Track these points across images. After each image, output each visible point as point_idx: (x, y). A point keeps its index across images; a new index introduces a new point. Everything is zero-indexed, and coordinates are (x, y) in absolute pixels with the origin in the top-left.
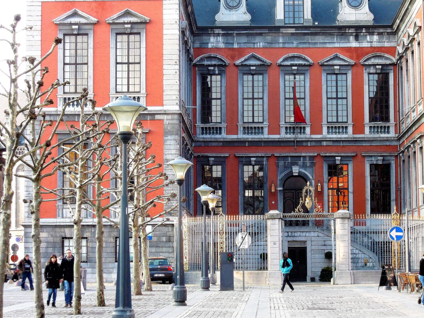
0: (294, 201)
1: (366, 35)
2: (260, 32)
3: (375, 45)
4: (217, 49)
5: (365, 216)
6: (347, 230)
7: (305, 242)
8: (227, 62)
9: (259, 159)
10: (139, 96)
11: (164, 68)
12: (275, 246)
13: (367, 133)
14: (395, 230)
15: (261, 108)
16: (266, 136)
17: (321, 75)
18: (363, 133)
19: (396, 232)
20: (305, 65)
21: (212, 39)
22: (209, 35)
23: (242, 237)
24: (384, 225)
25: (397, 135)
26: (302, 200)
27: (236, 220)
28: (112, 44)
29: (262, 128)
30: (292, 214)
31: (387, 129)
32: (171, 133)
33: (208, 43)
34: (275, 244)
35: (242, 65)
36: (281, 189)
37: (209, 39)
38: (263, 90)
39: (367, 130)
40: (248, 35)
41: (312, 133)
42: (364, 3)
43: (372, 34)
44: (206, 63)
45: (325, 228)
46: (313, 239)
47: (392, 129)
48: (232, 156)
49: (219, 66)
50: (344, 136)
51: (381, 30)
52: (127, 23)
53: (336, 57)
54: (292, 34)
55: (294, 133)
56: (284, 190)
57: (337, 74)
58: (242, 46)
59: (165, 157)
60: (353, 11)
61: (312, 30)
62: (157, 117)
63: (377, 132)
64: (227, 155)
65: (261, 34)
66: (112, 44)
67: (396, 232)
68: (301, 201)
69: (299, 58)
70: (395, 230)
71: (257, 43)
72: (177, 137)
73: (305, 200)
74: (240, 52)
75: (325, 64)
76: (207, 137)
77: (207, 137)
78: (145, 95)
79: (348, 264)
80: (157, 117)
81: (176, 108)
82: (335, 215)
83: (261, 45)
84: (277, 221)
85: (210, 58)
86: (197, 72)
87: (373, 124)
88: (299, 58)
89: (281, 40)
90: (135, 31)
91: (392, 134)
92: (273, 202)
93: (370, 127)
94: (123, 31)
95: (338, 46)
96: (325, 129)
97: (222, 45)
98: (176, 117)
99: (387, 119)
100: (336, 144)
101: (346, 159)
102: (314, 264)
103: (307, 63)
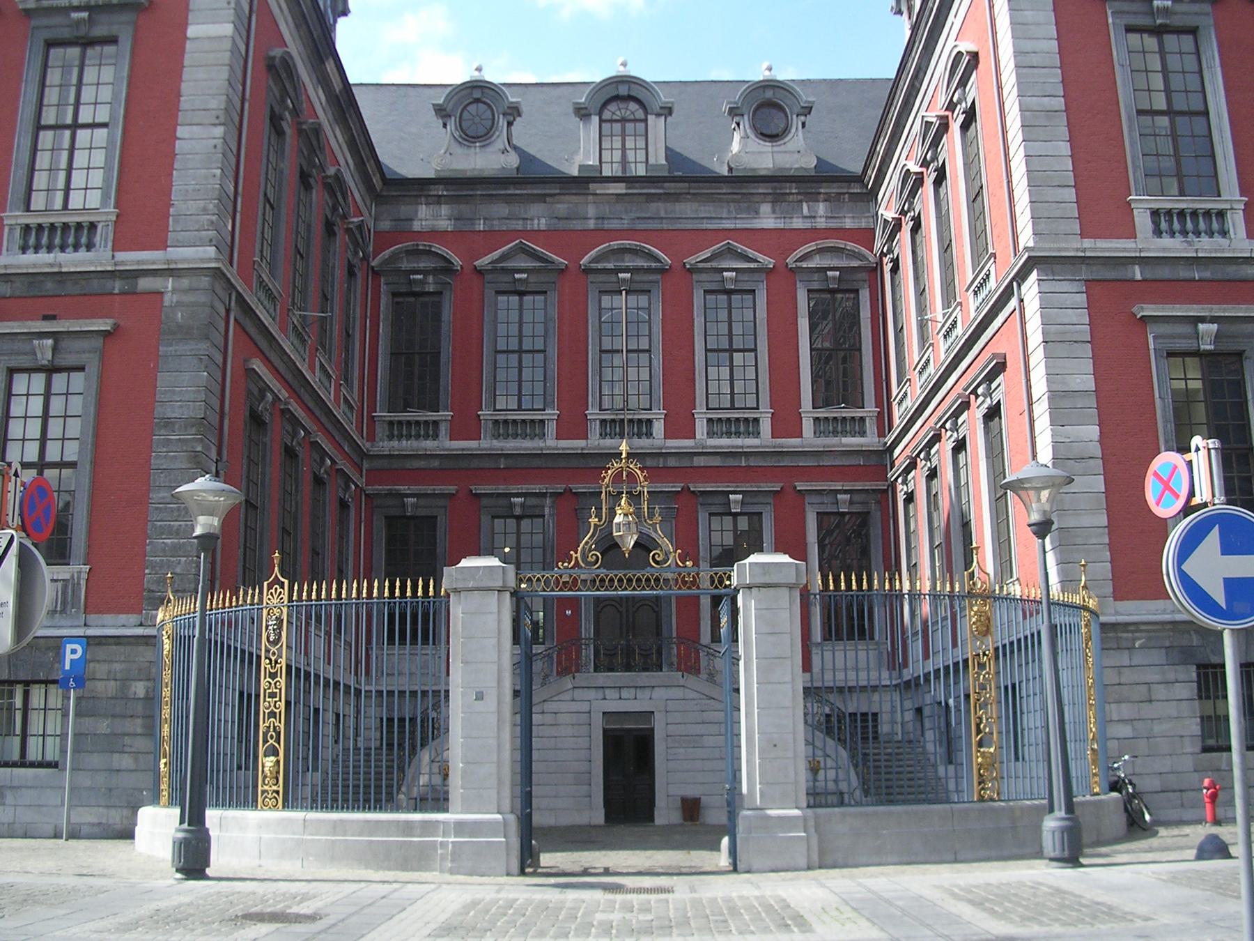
0: (623, 610)
1: (801, 201)
2: (539, 192)
3: (821, 223)
4: (435, 234)
6: (786, 639)
8: (457, 262)
9: (532, 501)
10: (92, 219)
11: (179, 134)
13: (809, 438)
14: (1214, 536)
15: (539, 375)
16: (551, 443)
17: (697, 512)
21: (423, 210)
22: (416, 200)
24: (857, 669)
26: (599, 516)
28: (31, 73)
31: (857, 425)
32: (184, 333)
33: (411, 220)
37: (416, 212)
38: (546, 331)
39: (808, 427)
40: (508, 199)
42: (793, 130)
43: (813, 197)
44: (405, 265)
45: (704, 676)
47: (871, 426)
49: (435, 271)
51: (834, 189)
57: (729, 292)
58: (497, 225)
59: (159, 411)
60: (767, 146)
61: (671, 187)
62: (144, 284)
64: (452, 489)
65: (542, 198)
66: (31, 73)
68: (593, 520)
70: (1214, 536)
71: (532, 219)
72: (203, 347)
73: (612, 514)
74: (493, 238)
75: (701, 265)
76: (408, 446)
77: (408, 446)
78: (114, 218)
80: (144, 284)
81: (206, 255)
82: (735, 575)
83: (543, 224)
85: (415, 253)
86: (383, 287)
87: (822, 413)
89: (591, 211)
90: (99, 31)
92: (569, 612)
94: (65, 33)
95: (732, 226)
96: (701, 428)
97: (445, 224)
98: (205, 281)
100: (730, 462)
101: (755, 500)
102: (671, 779)
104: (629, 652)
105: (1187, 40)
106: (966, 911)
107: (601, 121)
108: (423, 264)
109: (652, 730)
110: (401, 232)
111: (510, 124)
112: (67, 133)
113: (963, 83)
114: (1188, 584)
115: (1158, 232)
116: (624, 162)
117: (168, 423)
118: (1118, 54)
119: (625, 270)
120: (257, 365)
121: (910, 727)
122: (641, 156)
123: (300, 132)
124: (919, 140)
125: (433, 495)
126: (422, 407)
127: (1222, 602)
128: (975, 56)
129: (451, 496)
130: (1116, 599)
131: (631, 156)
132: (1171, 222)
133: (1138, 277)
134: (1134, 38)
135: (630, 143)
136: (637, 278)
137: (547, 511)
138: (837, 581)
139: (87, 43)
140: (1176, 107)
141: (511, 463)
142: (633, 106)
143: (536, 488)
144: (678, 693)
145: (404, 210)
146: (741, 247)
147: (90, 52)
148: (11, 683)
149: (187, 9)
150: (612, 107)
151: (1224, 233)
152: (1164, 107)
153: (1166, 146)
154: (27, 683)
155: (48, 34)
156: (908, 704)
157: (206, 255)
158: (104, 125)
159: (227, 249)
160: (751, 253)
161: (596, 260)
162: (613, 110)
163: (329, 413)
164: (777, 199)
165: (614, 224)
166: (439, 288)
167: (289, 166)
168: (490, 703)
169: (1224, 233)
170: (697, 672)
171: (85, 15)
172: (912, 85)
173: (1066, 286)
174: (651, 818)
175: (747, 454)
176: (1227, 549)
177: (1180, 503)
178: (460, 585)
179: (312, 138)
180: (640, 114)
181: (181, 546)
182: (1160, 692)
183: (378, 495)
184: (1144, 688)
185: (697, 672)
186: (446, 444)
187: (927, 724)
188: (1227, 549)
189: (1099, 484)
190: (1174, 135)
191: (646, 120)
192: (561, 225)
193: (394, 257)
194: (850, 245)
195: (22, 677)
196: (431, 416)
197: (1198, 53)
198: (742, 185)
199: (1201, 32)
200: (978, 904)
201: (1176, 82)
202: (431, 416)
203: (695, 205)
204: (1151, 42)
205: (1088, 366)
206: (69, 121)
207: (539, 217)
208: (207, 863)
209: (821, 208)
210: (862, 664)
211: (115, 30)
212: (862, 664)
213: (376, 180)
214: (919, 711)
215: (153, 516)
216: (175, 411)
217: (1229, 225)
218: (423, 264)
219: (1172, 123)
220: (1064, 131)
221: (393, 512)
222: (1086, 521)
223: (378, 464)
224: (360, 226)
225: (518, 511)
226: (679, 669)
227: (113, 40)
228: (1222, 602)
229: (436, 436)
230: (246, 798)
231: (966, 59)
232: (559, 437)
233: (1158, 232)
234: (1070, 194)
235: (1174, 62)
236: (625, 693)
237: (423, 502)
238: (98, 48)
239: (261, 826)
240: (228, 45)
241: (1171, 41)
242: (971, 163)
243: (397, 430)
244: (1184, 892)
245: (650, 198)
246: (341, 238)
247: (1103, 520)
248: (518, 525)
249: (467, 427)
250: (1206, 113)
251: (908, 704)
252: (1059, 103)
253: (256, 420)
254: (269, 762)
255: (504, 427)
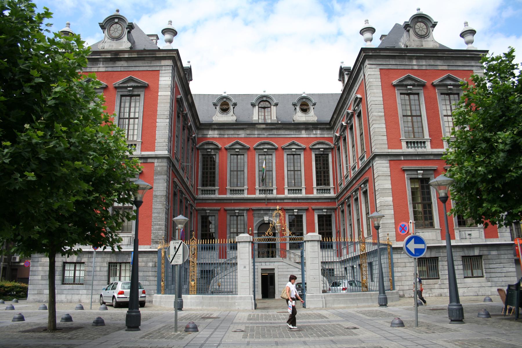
3: (319, 136)
4: (213, 138)
5: (331, 239)
7: (274, 269)
8: (220, 146)
9: (241, 212)
12: (245, 269)
14: (413, 240)
16: (246, 195)
18: (313, 193)
19: (415, 243)
20: (272, 149)
22: (208, 129)
23: (175, 248)
25: (335, 195)
27: (207, 243)
29: (243, 190)
30: (262, 237)
32: (160, 173)
34: (245, 267)
35: (230, 149)
36: (257, 232)
39: (315, 191)
41: (277, 194)
43: (316, 129)
44: (206, 147)
45: (288, 259)
46: (279, 267)
47: (332, 191)
48: (222, 210)
49: (214, 149)
50: (299, 196)
52: (130, 87)
53: (293, 144)
54: (264, 129)
55: (265, 194)
56: (258, 233)
57: (294, 155)
58: (230, 136)
63: (322, 193)
65: (243, 129)
67: (415, 243)
69: (268, 144)
70: (413, 240)
79: (249, 283)
80: (149, 160)
81: (165, 153)
83: (243, 136)
84: (247, 244)
86: (200, 153)
87: (319, 187)
88: (268, 144)
90: (136, 93)
91: (332, 194)
93: (317, 190)
94: (126, 93)
96: (286, 191)
98: (165, 160)
99: (328, 184)
103: (273, 147)
104: (268, 252)
105: (416, 96)
106: (361, 315)
107: (259, 107)
108: (211, 147)
109: (274, 274)
110: (204, 138)
111: (234, 108)
112: (127, 120)
113: (358, 105)
114: (407, 249)
115: (408, 147)
116: (265, 119)
117: (156, 196)
118: (398, 101)
119: (266, 149)
120: (176, 180)
121: (343, 272)
122: (269, 117)
123: (183, 116)
124: (345, 117)
125: (214, 210)
126: (210, 186)
127: (414, 253)
128: (361, 99)
129: (219, 210)
130: (397, 241)
131: (267, 117)
132: (411, 144)
133: (403, 159)
134: (402, 96)
135: (266, 114)
136: (269, 151)
137: (245, 214)
138: (329, 239)
139: (131, 96)
140: (413, 114)
141: (235, 201)
142: (267, 103)
143: (242, 208)
144: (281, 263)
145: (205, 132)
146: (297, 142)
147: (132, 98)
148: (116, 263)
149: (158, 88)
150: (262, 103)
151: (425, 147)
152: (410, 114)
153: (410, 124)
154: (121, 263)
155: (122, 93)
156: (343, 266)
157: (165, 153)
158: (137, 118)
159: (169, 151)
160: (299, 144)
161: (258, 146)
162: (262, 104)
163: (188, 189)
164: (306, 129)
165: (262, 136)
166: (215, 153)
167: (180, 126)
168: (247, 268)
169: (425, 147)
170: (286, 258)
171: (131, 89)
172: (344, 102)
173: (384, 162)
174: (274, 297)
175: (299, 199)
176: (415, 243)
177: (406, 232)
178: (240, 241)
179: (185, 117)
180: (269, 106)
181: (160, 228)
182: (408, 264)
183: (199, 210)
184: (404, 264)
185: (286, 258)
186: (217, 196)
187: (348, 272)
188: (415, 243)
189: (392, 212)
190: (412, 122)
191: (270, 107)
192: (248, 136)
193: (203, 145)
194: (327, 142)
195: (120, 261)
196: (213, 188)
197: (419, 100)
198: (297, 126)
199: (420, 94)
200: (364, 314)
201: (413, 108)
202: (213, 188)
203: (284, 131)
204: (407, 97)
205: (390, 182)
206: (127, 117)
207: (242, 134)
208: (182, 307)
209: (319, 132)
210: (329, 256)
211: (139, 93)
212: (329, 256)
213: (198, 124)
214: (346, 268)
215: (153, 220)
216: (158, 193)
217: (426, 145)
218: (211, 147)
219: (412, 119)
220: (384, 121)
221: (203, 214)
222: (389, 221)
223: (199, 201)
224: (195, 137)
225: (237, 214)
226: (281, 257)
227: (139, 95)
228: (414, 253)
229: (215, 194)
230: (188, 292)
231: (359, 99)
232: (248, 194)
233: (408, 147)
234: (385, 138)
235: (413, 102)
236: (267, 264)
237: (211, 212)
238: (134, 98)
239: (191, 298)
240: (169, 98)
241: (412, 97)
242: (360, 124)
243: (204, 192)
244: (409, 312)
245: (272, 129)
246: (191, 141)
247: (393, 221)
248: (237, 218)
249: (223, 191)
250: (421, 116)
251: (343, 266)
252: (383, 114)
253: (175, 194)
254: (193, 283)
255: (233, 191)
